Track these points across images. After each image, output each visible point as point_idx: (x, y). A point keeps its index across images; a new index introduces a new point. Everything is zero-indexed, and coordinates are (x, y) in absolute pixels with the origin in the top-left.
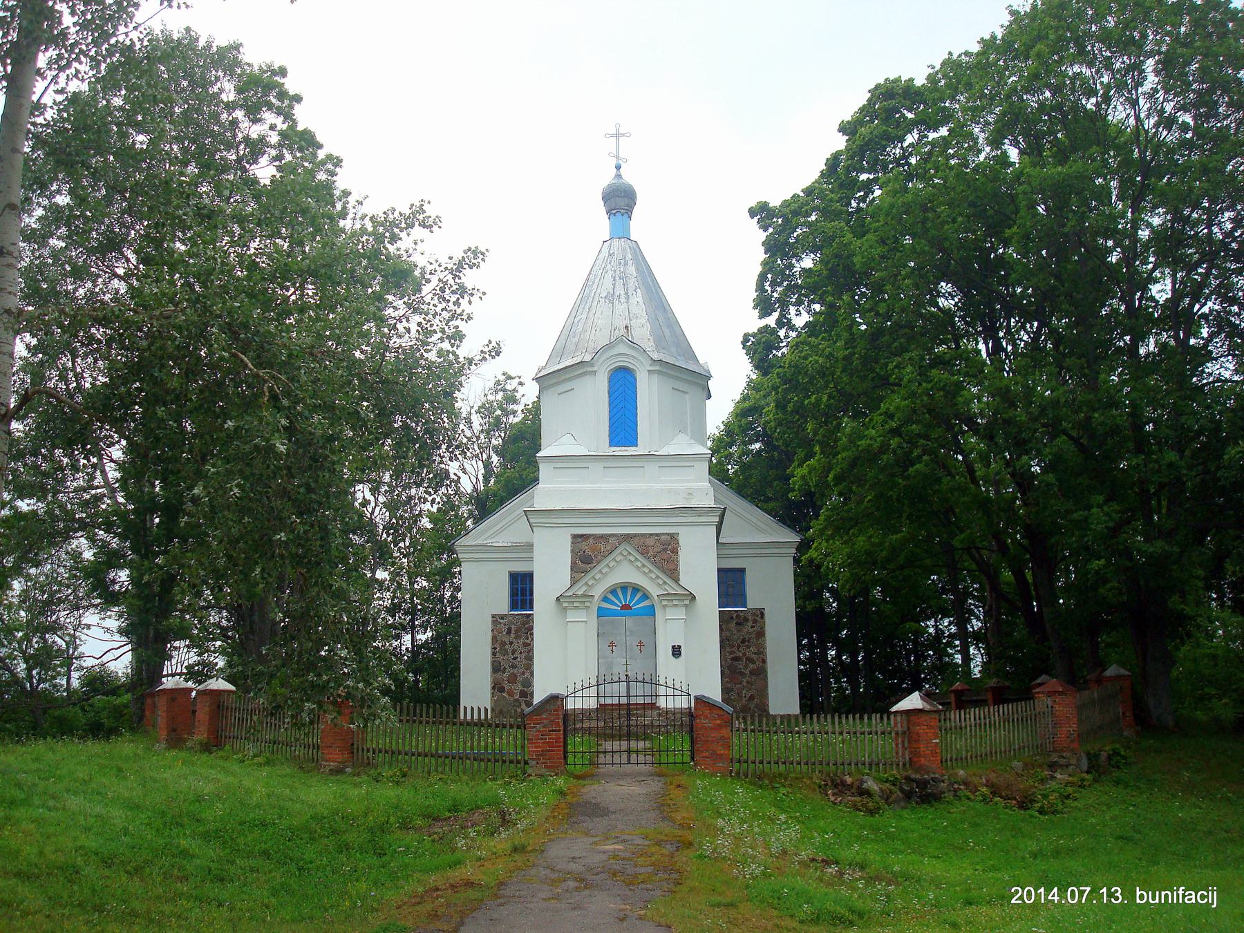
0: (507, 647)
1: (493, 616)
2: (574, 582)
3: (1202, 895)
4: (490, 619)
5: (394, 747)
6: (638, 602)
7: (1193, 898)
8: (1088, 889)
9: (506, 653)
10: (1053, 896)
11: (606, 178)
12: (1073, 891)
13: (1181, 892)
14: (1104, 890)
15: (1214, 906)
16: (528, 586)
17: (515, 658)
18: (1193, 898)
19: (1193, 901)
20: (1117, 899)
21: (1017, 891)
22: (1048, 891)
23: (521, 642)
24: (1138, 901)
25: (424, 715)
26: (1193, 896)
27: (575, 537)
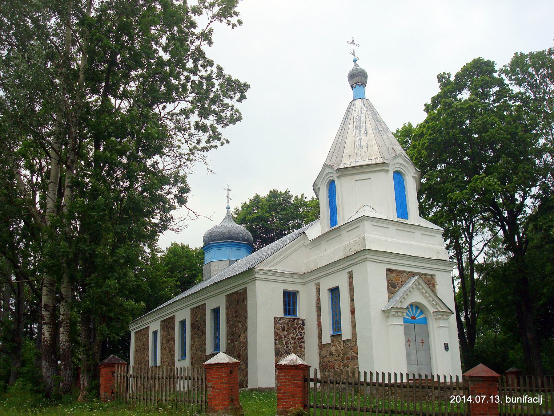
0: (283, 339)
1: (275, 318)
3: (535, 399)
4: (273, 320)
6: (419, 315)
7: (531, 400)
8: (485, 396)
9: (282, 344)
10: (469, 399)
11: (350, 67)
12: (478, 397)
13: (526, 398)
14: (492, 397)
15: (541, 404)
16: (287, 308)
17: (288, 347)
18: (531, 400)
19: (531, 402)
20: (497, 401)
21: (453, 397)
22: (466, 398)
23: (291, 336)
24: (507, 402)
25: (287, 309)
26: (531, 400)
27: (388, 270)
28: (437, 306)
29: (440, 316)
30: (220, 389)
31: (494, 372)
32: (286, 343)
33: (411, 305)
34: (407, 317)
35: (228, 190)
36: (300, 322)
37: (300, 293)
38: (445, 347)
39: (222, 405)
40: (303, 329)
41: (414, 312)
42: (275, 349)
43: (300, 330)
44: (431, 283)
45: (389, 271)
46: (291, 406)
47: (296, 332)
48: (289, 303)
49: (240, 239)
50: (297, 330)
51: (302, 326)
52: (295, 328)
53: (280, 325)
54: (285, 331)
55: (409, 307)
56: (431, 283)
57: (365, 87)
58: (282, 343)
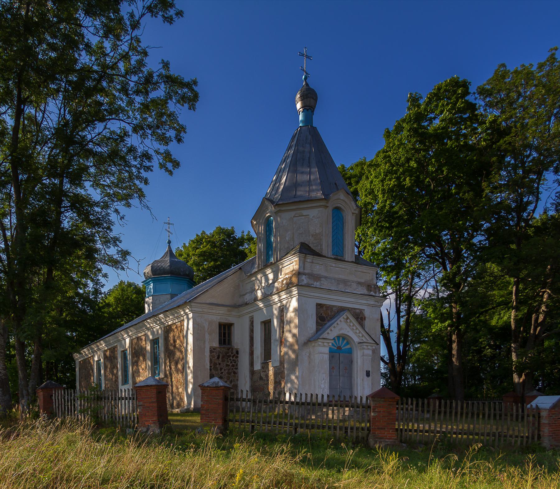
0: (217, 366)
2: (317, 330)
6: (345, 345)
17: (222, 373)
29: (365, 347)
30: (149, 407)
32: (221, 369)
33: (338, 337)
34: (333, 347)
36: (234, 352)
37: (235, 325)
38: (367, 374)
39: (152, 421)
41: (341, 343)
43: (234, 358)
45: (319, 306)
46: (213, 420)
47: (230, 359)
48: (225, 334)
49: (182, 273)
50: (231, 358)
51: (236, 355)
52: (229, 356)
53: (215, 354)
54: (220, 359)
55: (336, 339)
57: (313, 112)
58: (216, 369)
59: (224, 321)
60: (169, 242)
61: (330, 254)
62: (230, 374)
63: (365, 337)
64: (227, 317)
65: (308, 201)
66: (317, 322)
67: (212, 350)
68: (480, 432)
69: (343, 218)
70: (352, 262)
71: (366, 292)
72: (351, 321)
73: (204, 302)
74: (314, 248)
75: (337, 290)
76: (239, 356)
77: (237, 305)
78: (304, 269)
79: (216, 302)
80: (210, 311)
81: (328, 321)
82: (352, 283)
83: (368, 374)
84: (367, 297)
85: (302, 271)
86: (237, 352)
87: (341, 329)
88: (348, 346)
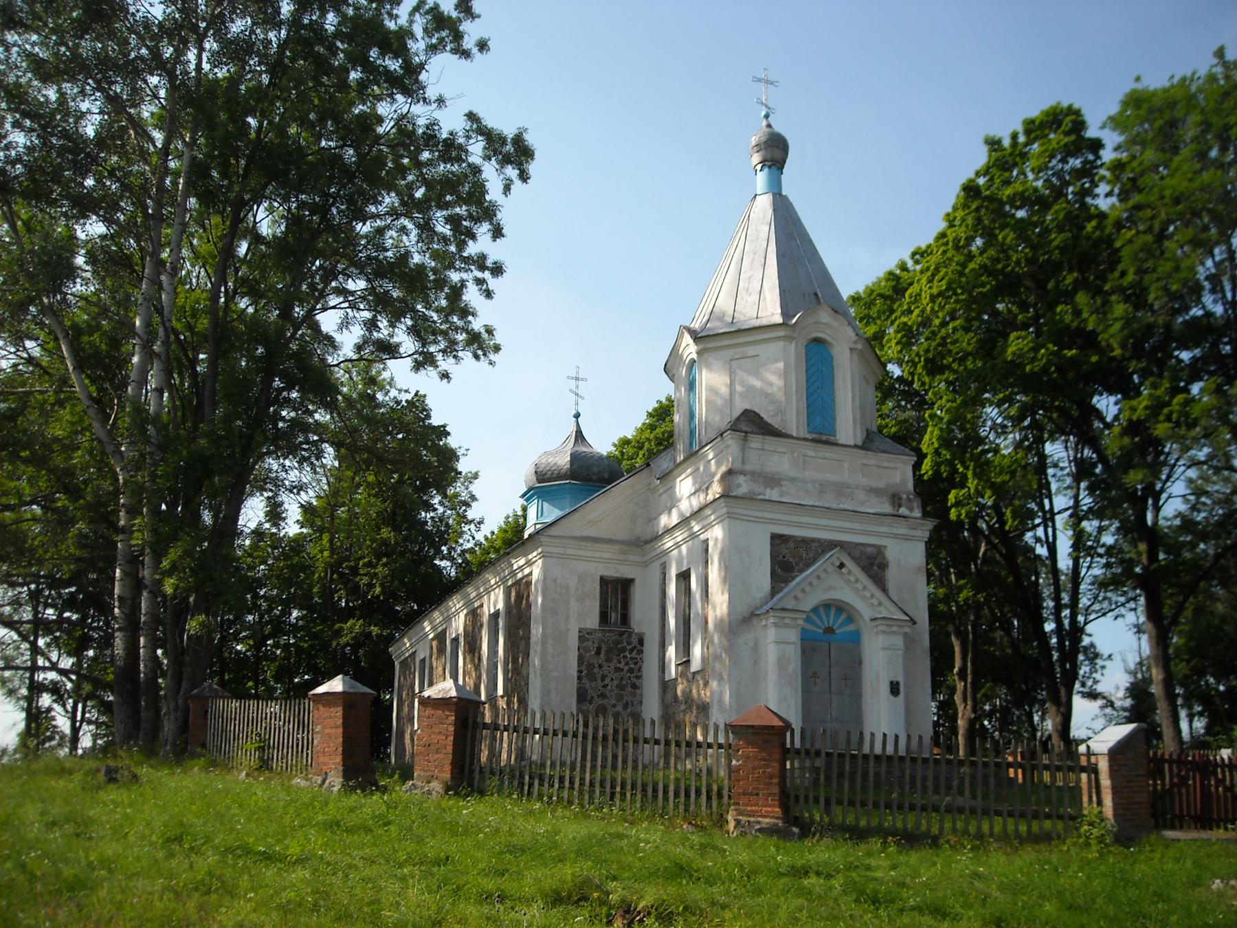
0: (596, 670)
2: (774, 591)
5: (710, 739)
6: (843, 625)
17: (605, 686)
23: (612, 665)
27: (774, 537)
28: (881, 609)
31: (359, 685)
32: (603, 678)
33: (827, 606)
35: (577, 379)
36: (635, 642)
40: (640, 652)
41: (831, 620)
42: (578, 689)
44: (877, 562)
45: (777, 539)
47: (625, 657)
49: (594, 477)
50: (627, 653)
51: (639, 647)
52: (623, 650)
53: (590, 643)
54: (602, 655)
56: (877, 562)
58: (592, 677)
59: (613, 572)
60: (577, 416)
61: (804, 433)
62: (623, 690)
63: (885, 607)
64: (618, 566)
65: (755, 328)
66: (773, 573)
67: (584, 636)
68: (967, 806)
69: (832, 359)
70: (856, 446)
71: (887, 508)
72: (850, 572)
73: (568, 534)
74: (769, 421)
75: (821, 504)
76: (644, 649)
77: (643, 539)
78: (743, 463)
79: (594, 535)
80: (581, 553)
81: (801, 571)
82: (856, 491)
83: (894, 689)
84: (889, 519)
85: (738, 466)
86: (641, 642)
87: (829, 588)
88: (851, 627)
